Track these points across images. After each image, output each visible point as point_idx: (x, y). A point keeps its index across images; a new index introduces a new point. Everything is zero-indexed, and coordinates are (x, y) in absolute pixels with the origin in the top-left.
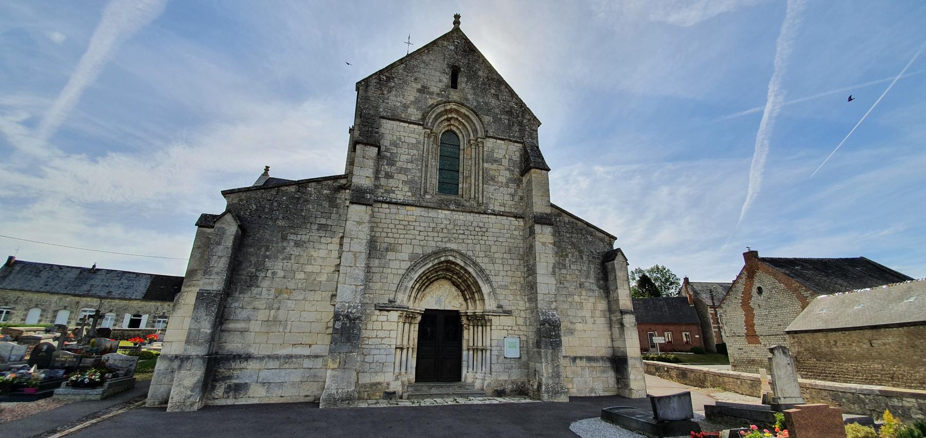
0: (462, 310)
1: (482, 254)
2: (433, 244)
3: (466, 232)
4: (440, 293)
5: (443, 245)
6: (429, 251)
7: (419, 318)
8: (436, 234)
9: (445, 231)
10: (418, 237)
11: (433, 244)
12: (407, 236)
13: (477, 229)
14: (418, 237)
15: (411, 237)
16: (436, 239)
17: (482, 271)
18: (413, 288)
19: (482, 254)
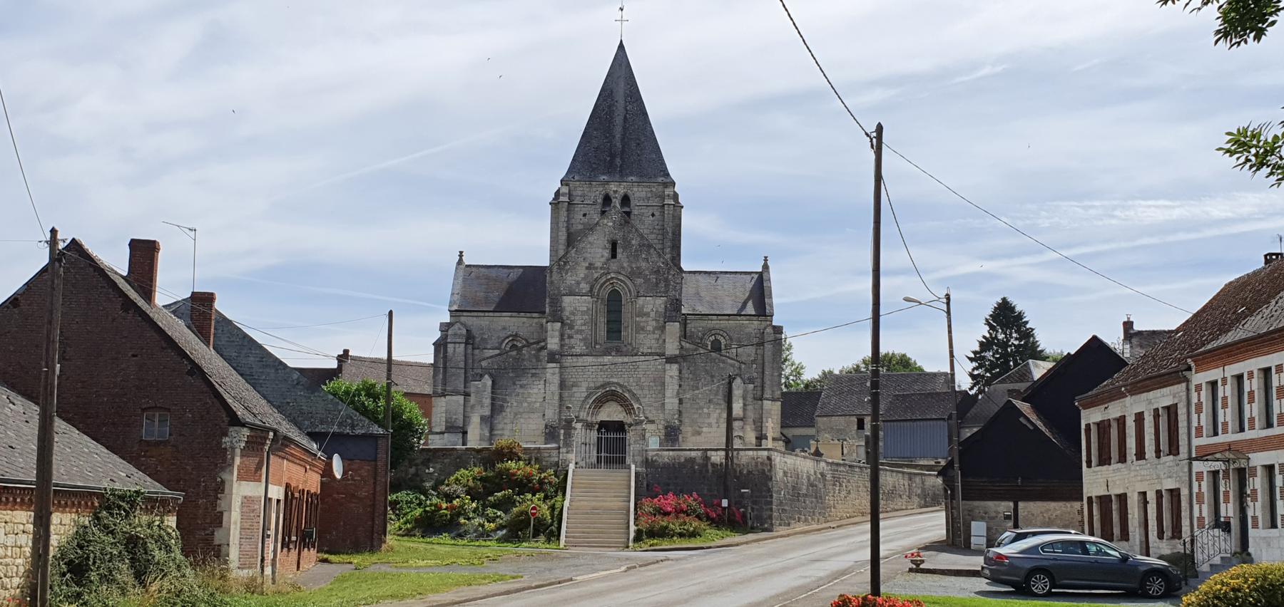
0: (625, 420)
1: (634, 384)
2: (601, 380)
3: (624, 370)
4: (611, 409)
5: (608, 380)
6: (599, 384)
7: (597, 426)
8: (603, 373)
9: (609, 370)
10: (591, 377)
11: (601, 380)
12: (584, 376)
13: (631, 367)
14: (591, 377)
15: (587, 376)
16: (603, 376)
17: (634, 395)
18: (590, 408)
19: (634, 384)
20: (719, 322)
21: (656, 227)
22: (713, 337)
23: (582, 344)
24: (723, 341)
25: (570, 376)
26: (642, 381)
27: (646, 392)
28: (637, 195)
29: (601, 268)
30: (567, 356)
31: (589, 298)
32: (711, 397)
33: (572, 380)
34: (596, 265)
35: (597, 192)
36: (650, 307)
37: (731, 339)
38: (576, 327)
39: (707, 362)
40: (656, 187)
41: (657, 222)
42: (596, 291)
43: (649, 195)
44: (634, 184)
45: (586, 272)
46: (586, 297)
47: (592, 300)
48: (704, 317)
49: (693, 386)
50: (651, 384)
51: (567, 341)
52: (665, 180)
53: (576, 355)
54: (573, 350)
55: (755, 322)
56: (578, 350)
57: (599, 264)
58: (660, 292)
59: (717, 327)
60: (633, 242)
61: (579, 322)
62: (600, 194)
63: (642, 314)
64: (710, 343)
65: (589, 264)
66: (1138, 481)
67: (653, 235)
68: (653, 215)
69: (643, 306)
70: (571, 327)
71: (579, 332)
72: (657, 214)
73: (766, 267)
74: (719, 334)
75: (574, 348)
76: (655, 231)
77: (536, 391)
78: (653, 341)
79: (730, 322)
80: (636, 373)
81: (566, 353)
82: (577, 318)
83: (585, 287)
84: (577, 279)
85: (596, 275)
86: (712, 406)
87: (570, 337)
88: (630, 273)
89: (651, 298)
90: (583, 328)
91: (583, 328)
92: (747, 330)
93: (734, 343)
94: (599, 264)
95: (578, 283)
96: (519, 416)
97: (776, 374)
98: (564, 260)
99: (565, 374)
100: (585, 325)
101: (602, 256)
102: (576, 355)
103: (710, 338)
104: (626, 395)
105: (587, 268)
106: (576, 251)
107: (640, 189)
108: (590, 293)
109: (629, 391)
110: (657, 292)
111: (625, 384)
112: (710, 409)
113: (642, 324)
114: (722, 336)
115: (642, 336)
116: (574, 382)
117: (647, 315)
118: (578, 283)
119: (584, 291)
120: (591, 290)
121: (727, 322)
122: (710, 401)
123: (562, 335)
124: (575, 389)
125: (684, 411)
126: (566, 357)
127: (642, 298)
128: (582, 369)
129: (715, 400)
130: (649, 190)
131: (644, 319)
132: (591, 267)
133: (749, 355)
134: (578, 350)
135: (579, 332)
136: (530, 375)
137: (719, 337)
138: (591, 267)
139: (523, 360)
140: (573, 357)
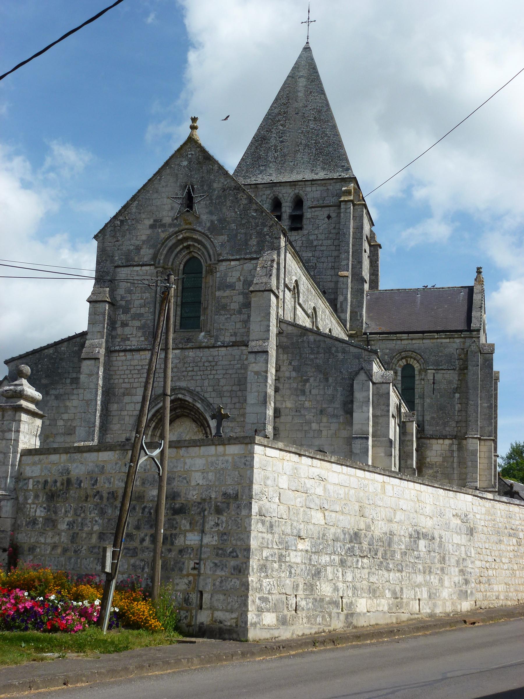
3: (196, 369)
20: (410, 341)
21: (333, 231)
22: (404, 361)
23: (140, 334)
24: (416, 366)
25: (121, 381)
26: (221, 384)
27: (226, 400)
28: (310, 196)
29: (170, 225)
30: (119, 351)
31: (152, 268)
32: (324, 406)
33: (124, 385)
34: (164, 222)
35: (265, 197)
36: (236, 274)
37: (426, 362)
38: (133, 311)
39: (318, 353)
40: (333, 184)
41: (334, 225)
42: (162, 257)
43: (325, 194)
44: (307, 183)
45: (149, 232)
46: (148, 268)
47: (155, 271)
48: (392, 336)
49: (296, 389)
50: (234, 388)
51: (119, 331)
52: (344, 175)
53: (131, 350)
54: (128, 343)
55: (458, 341)
56: (134, 343)
57: (167, 220)
58: (251, 253)
59: (408, 348)
60: (215, 185)
61: (137, 303)
62: (267, 198)
63: (225, 286)
64: (400, 369)
65: (155, 221)
66: (330, 621)
67: (329, 241)
68: (329, 217)
69: (226, 275)
70: (126, 311)
71: (138, 316)
72: (333, 215)
73: (479, 280)
74: (411, 357)
75: (128, 339)
76: (331, 236)
77: (75, 403)
78: (239, 325)
79: (424, 341)
80: (214, 372)
81: (117, 348)
82: (134, 297)
83: (147, 253)
84: (138, 243)
85: (163, 236)
86: (325, 420)
87: (124, 325)
88: (209, 229)
89: (237, 263)
90: (143, 310)
91: (143, 310)
92: (447, 351)
93: (431, 367)
94: (167, 220)
95: (138, 249)
96: (52, 439)
97: (486, 405)
98: (121, 218)
99: (114, 377)
100: (145, 306)
101: (172, 208)
102: (131, 350)
103: (400, 362)
104: (199, 406)
105: (152, 227)
106: (138, 204)
107: (314, 189)
108: (154, 262)
109: (203, 400)
110: (246, 254)
111: (198, 389)
112: (322, 424)
113: (223, 300)
114: (415, 359)
115: (223, 318)
116: (126, 389)
117: (231, 286)
118: (138, 249)
119: (145, 259)
120: (155, 257)
121: (421, 341)
122: (322, 412)
123: (112, 324)
124: (127, 399)
125: (281, 428)
126: (117, 354)
127: (224, 263)
128: (138, 370)
129: (330, 410)
130: (326, 188)
131: (228, 293)
132: (157, 224)
133: (450, 382)
134: (134, 343)
135: (138, 316)
136: (68, 381)
137: (412, 362)
138: (157, 224)
139: (61, 359)
140: (127, 353)
